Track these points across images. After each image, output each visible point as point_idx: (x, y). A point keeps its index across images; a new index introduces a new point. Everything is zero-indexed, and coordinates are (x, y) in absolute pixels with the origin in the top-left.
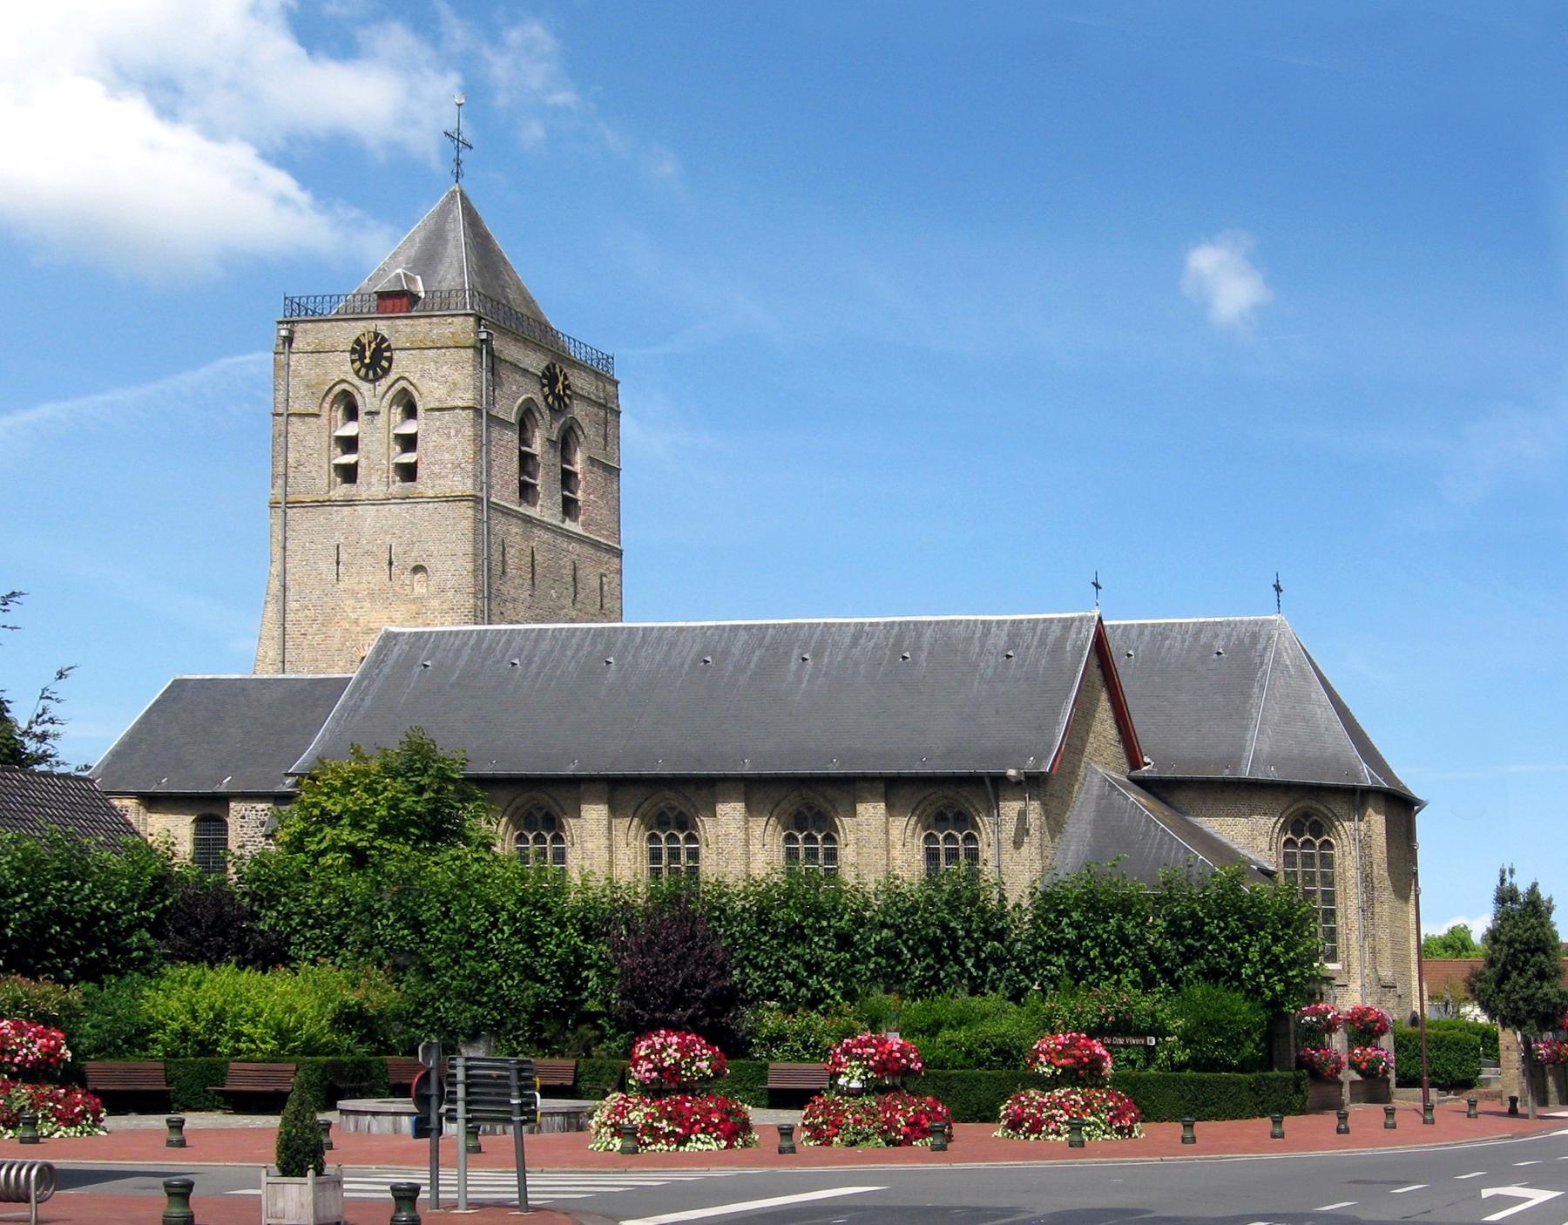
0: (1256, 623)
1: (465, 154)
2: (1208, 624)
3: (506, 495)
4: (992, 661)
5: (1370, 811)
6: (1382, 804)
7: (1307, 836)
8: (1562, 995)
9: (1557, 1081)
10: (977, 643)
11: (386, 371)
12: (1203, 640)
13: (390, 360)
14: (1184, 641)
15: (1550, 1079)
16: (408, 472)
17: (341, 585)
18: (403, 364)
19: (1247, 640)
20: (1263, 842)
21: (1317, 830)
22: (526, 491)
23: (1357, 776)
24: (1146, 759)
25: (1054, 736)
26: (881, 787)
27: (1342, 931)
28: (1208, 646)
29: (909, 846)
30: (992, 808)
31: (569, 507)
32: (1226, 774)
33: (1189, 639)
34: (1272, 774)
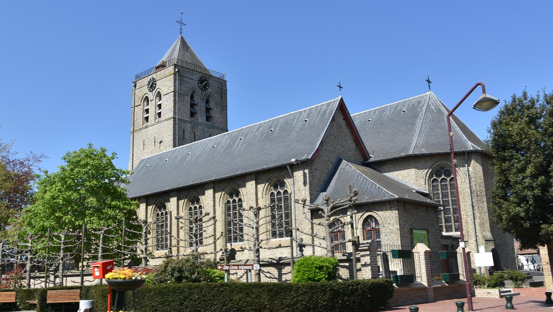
0: (420, 97)
1: (183, 27)
2: (401, 102)
3: (187, 117)
4: (300, 124)
5: (473, 161)
6: (479, 159)
7: (443, 177)
8: (552, 197)
9: (118, 295)
10: (296, 119)
11: (155, 88)
12: (398, 108)
13: (156, 84)
14: (391, 110)
15: (117, 294)
16: (159, 114)
17: (145, 151)
18: (159, 84)
19: (416, 104)
20: (422, 181)
21: (448, 174)
22: (192, 114)
23: (466, 147)
24: (371, 156)
25: (316, 144)
26: (254, 176)
27: (464, 217)
28: (400, 110)
29: (264, 198)
30: (291, 176)
31: (208, 118)
32: (403, 154)
33: (393, 109)
34: (424, 151)
